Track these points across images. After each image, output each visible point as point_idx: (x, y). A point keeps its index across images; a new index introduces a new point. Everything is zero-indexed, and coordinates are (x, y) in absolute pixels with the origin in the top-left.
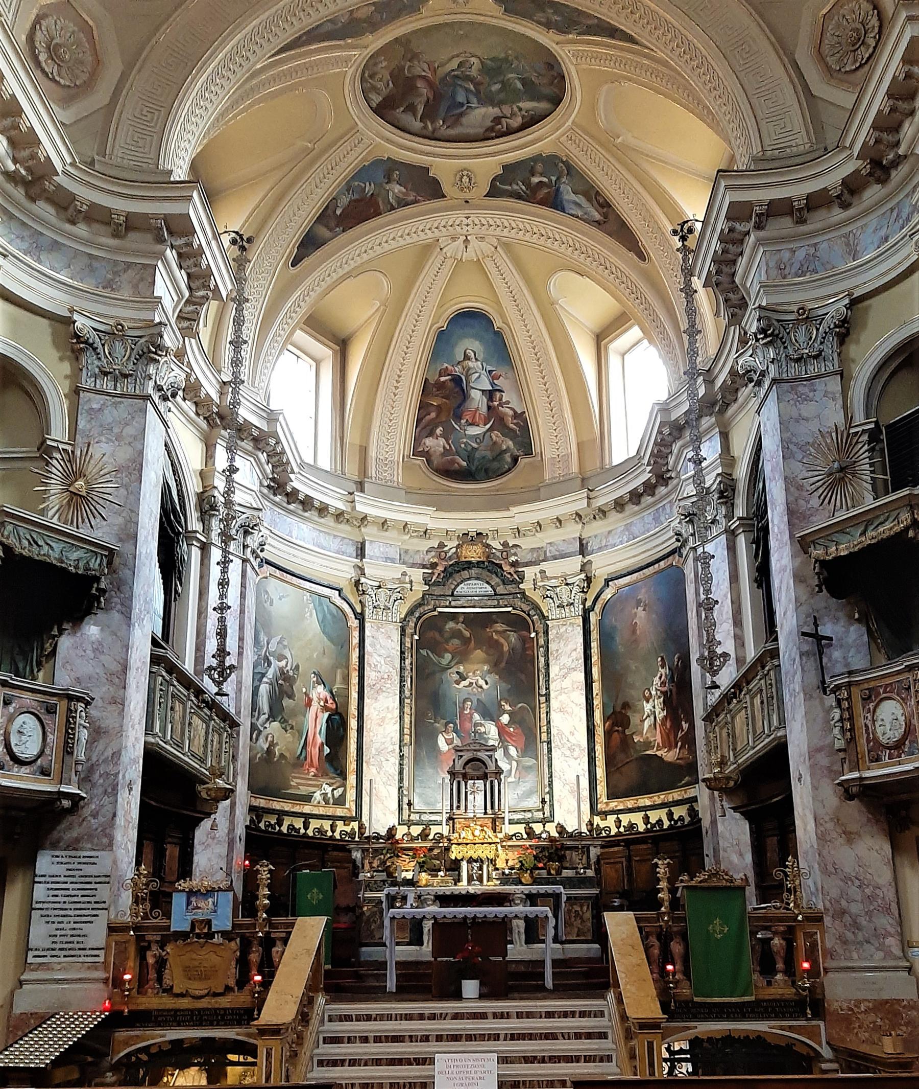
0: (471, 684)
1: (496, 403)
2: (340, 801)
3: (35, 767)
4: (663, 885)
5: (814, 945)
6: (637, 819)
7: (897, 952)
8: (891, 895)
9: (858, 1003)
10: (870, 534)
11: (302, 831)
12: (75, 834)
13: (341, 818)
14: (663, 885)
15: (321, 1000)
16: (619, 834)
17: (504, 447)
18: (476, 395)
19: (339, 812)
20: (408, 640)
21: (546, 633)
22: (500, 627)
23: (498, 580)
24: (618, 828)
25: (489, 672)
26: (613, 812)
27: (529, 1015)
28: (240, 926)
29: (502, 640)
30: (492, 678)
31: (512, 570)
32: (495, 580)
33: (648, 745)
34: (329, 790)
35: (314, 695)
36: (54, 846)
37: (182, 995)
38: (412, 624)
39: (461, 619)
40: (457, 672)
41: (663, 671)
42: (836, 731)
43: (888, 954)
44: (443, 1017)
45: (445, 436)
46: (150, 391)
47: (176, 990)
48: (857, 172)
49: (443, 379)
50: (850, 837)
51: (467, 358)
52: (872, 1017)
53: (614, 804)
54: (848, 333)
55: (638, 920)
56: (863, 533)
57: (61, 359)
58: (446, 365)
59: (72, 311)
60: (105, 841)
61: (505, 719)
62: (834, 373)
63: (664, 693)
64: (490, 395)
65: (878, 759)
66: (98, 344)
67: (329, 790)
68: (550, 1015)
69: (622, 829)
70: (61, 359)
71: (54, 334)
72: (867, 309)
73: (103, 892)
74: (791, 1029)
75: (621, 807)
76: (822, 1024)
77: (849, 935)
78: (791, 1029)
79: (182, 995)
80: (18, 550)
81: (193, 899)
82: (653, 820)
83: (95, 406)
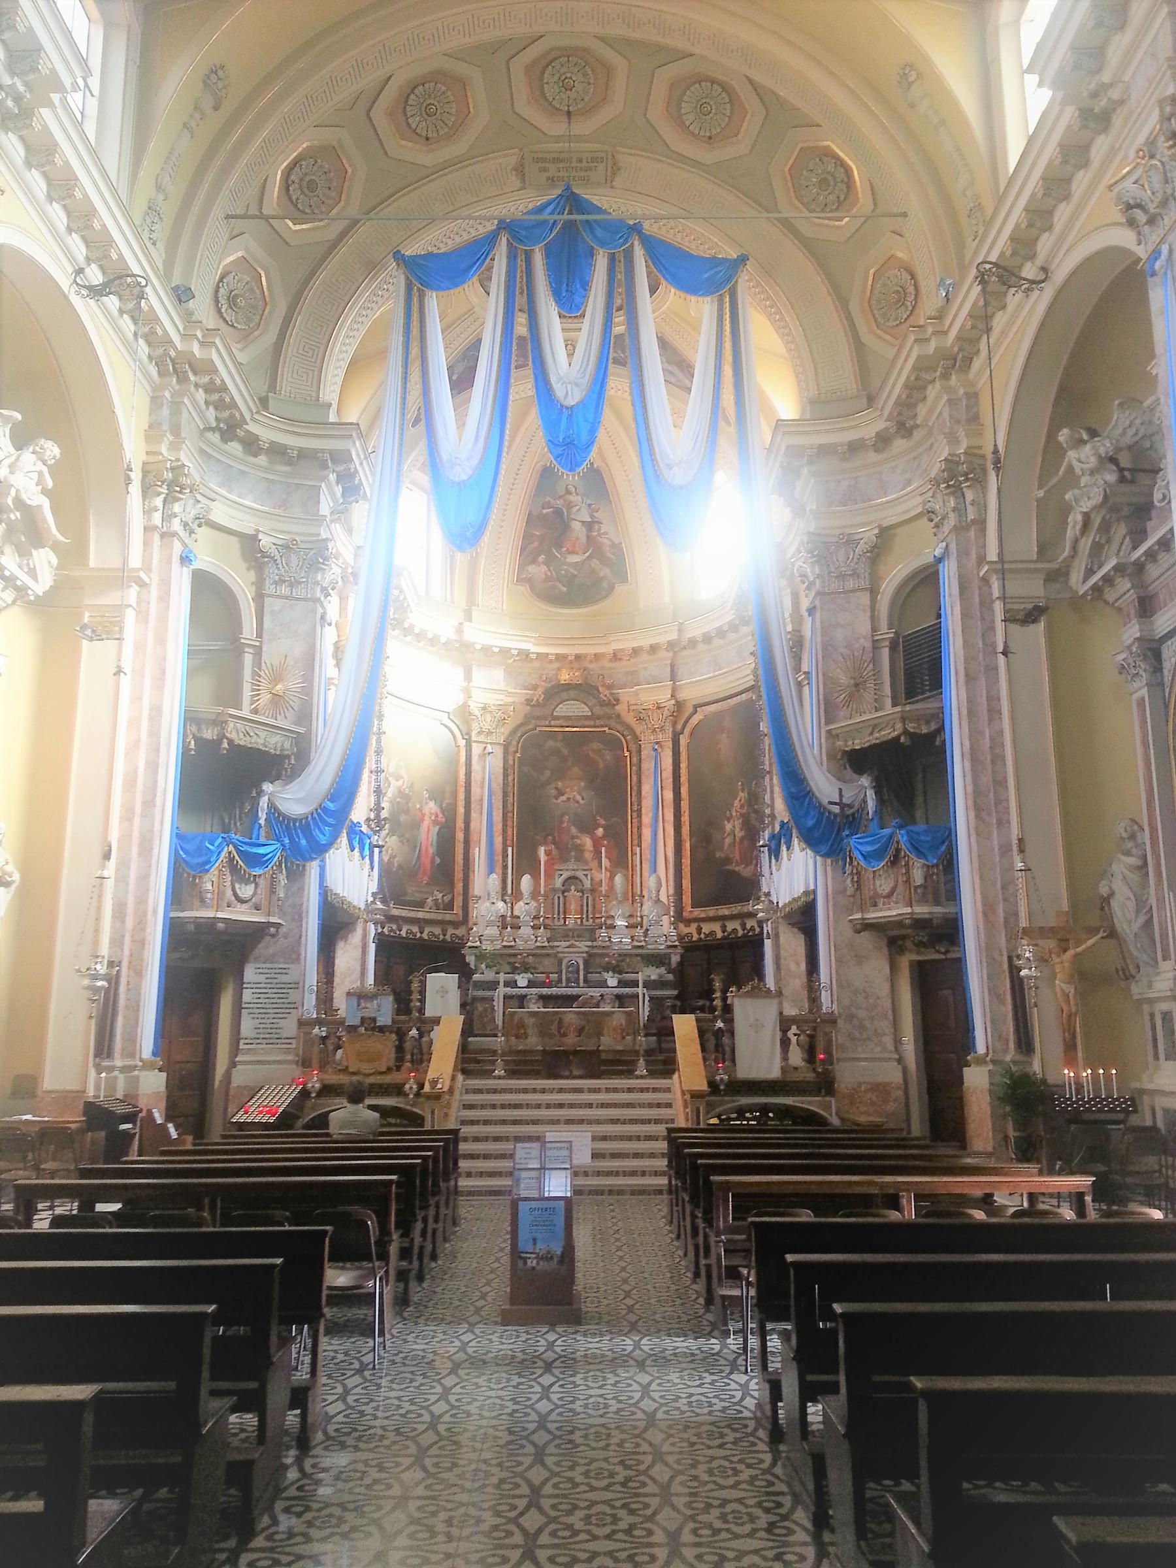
0: (568, 799)
1: (595, 534)
2: (450, 906)
3: (250, 904)
4: (718, 994)
5: (829, 1042)
6: (716, 927)
7: (891, 1047)
8: (888, 1004)
9: (860, 1084)
10: (877, 735)
11: (418, 935)
12: (271, 951)
13: (450, 923)
14: (718, 994)
15: (460, 1077)
16: (700, 940)
17: (602, 575)
18: (576, 526)
19: (448, 917)
20: (511, 758)
21: (639, 751)
22: (595, 745)
23: (594, 701)
24: (699, 934)
25: (586, 788)
26: (696, 920)
27: (615, 1090)
28: (399, 1022)
29: (597, 758)
30: (589, 794)
31: (607, 692)
32: (591, 702)
33: (727, 860)
34: (439, 896)
35: (426, 810)
36: (256, 960)
37: (354, 1073)
38: (514, 743)
39: (560, 738)
40: (556, 788)
41: (742, 794)
42: (849, 881)
43: (885, 1049)
44: (551, 1091)
45: (547, 563)
46: (318, 594)
47: (351, 1070)
48: (886, 429)
49: (545, 511)
50: (860, 959)
51: (568, 492)
52: (869, 1095)
53: (698, 913)
54: (878, 555)
55: (698, 1020)
56: (871, 734)
57: (248, 569)
58: (548, 499)
59: (258, 531)
60: (294, 956)
61: (600, 832)
62: (866, 589)
63: (742, 815)
64: (589, 526)
65: (875, 905)
66: (278, 557)
67: (439, 896)
68: (630, 1090)
69: (702, 936)
70: (248, 569)
71: (243, 548)
72: (895, 535)
73: (294, 996)
74: (809, 1103)
75: (703, 915)
76: (833, 1101)
77: (857, 1034)
78: (809, 1103)
79: (354, 1073)
80: (237, 742)
81: (362, 1001)
82: (729, 929)
83: (277, 608)
